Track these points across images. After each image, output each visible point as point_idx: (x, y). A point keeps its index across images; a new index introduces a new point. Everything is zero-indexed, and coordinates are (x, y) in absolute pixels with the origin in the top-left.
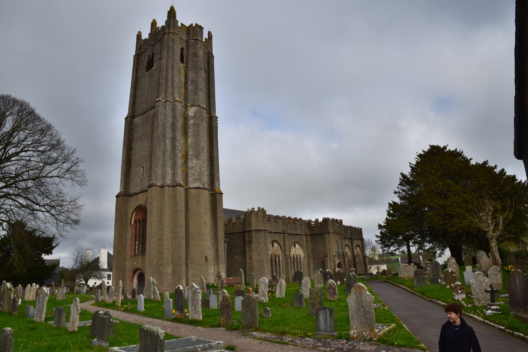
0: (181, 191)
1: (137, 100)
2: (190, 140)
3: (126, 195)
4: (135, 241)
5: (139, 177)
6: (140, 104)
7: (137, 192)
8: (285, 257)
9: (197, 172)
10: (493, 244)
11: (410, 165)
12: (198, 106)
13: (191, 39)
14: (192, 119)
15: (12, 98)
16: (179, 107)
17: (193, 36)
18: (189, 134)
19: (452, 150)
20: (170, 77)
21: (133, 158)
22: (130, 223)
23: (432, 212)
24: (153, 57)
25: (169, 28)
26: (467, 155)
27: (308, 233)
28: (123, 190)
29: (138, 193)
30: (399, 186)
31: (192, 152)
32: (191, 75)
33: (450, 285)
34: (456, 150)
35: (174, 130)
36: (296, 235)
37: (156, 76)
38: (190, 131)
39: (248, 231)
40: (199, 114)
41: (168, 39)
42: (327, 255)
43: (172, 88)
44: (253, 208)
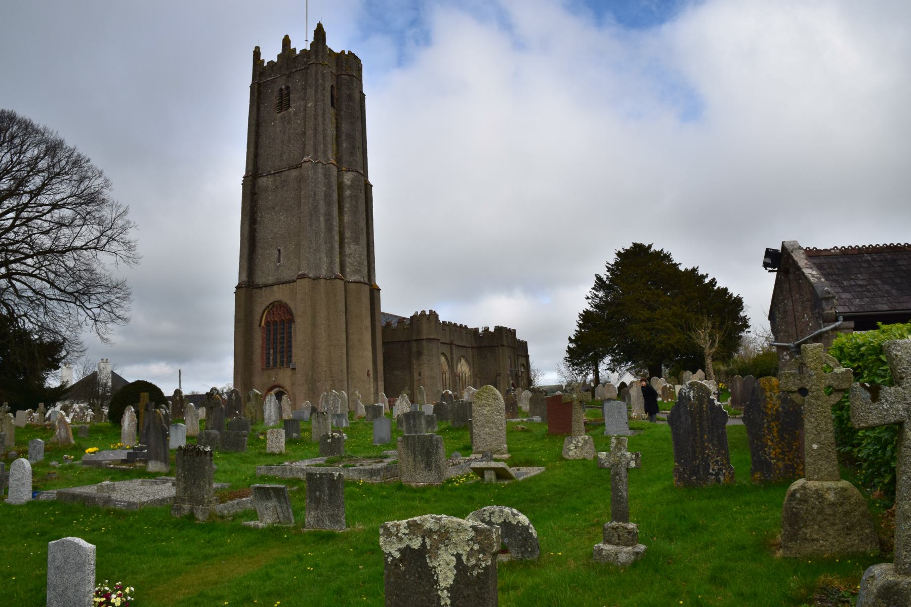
0: (340, 284)
1: (261, 151)
2: (346, 218)
3: (251, 286)
4: (269, 349)
5: (273, 263)
6: (267, 158)
8: (453, 374)
9: (357, 260)
10: (709, 361)
11: (607, 265)
13: (344, 73)
14: (349, 189)
16: (334, 170)
17: (346, 70)
18: (346, 209)
19: (657, 251)
20: (320, 128)
21: (259, 235)
22: (260, 325)
23: (638, 325)
24: (288, 94)
25: (317, 56)
26: (676, 259)
27: (474, 345)
28: (244, 278)
29: (272, 285)
30: (593, 291)
31: (350, 234)
32: (345, 127)
33: (668, 400)
34: (662, 250)
35: (329, 204)
36: (462, 346)
37: (297, 123)
38: (347, 206)
39: (417, 340)
40: (357, 183)
41: (316, 72)
42: (500, 373)
43: (324, 144)
44: (424, 311)
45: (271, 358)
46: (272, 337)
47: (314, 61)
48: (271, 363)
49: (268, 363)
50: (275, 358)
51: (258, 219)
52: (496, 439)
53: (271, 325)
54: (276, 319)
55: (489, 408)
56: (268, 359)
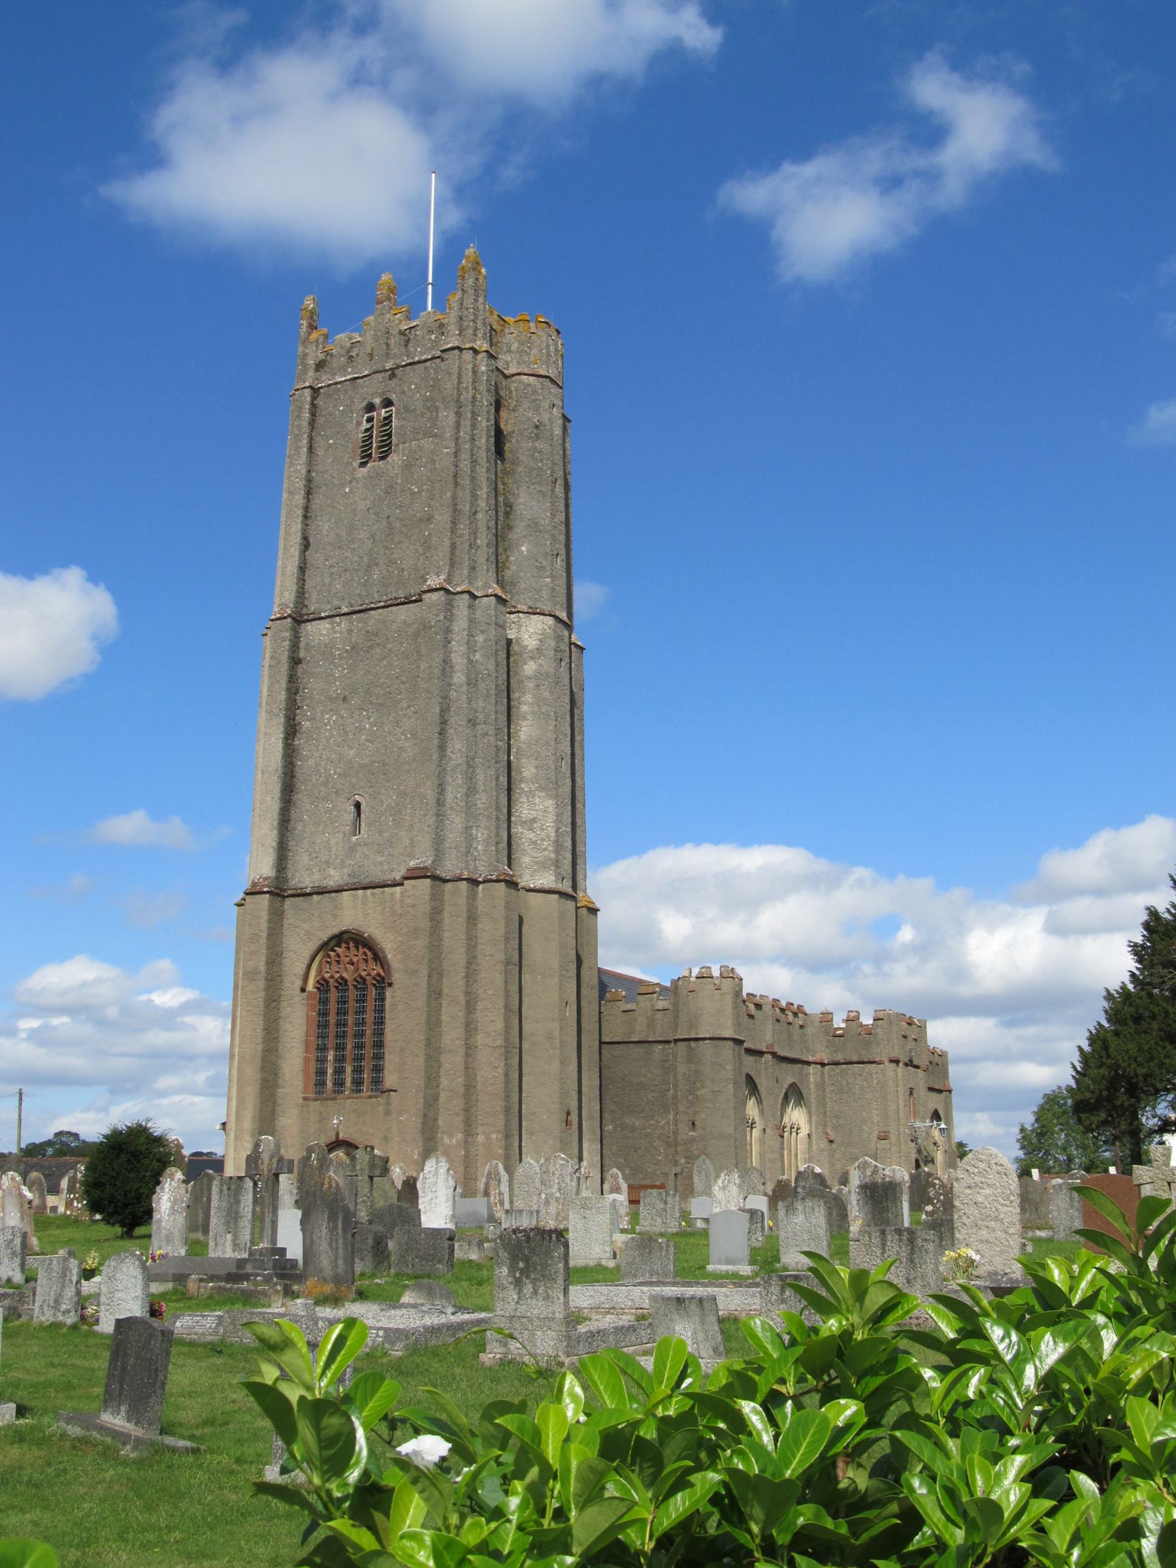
4: (322, 1049)
7: (331, 883)
12: (550, 615)
15: (1096, 1029)
18: (524, 708)
22: (303, 990)
29: (339, 891)
45: (330, 1071)
46: (332, 1019)
47: (457, 344)
48: (329, 1084)
49: (321, 1084)
50: (339, 1071)
51: (306, 724)
52: (1001, 1252)
53: (333, 989)
54: (345, 975)
55: (987, 1191)
56: (321, 1072)
